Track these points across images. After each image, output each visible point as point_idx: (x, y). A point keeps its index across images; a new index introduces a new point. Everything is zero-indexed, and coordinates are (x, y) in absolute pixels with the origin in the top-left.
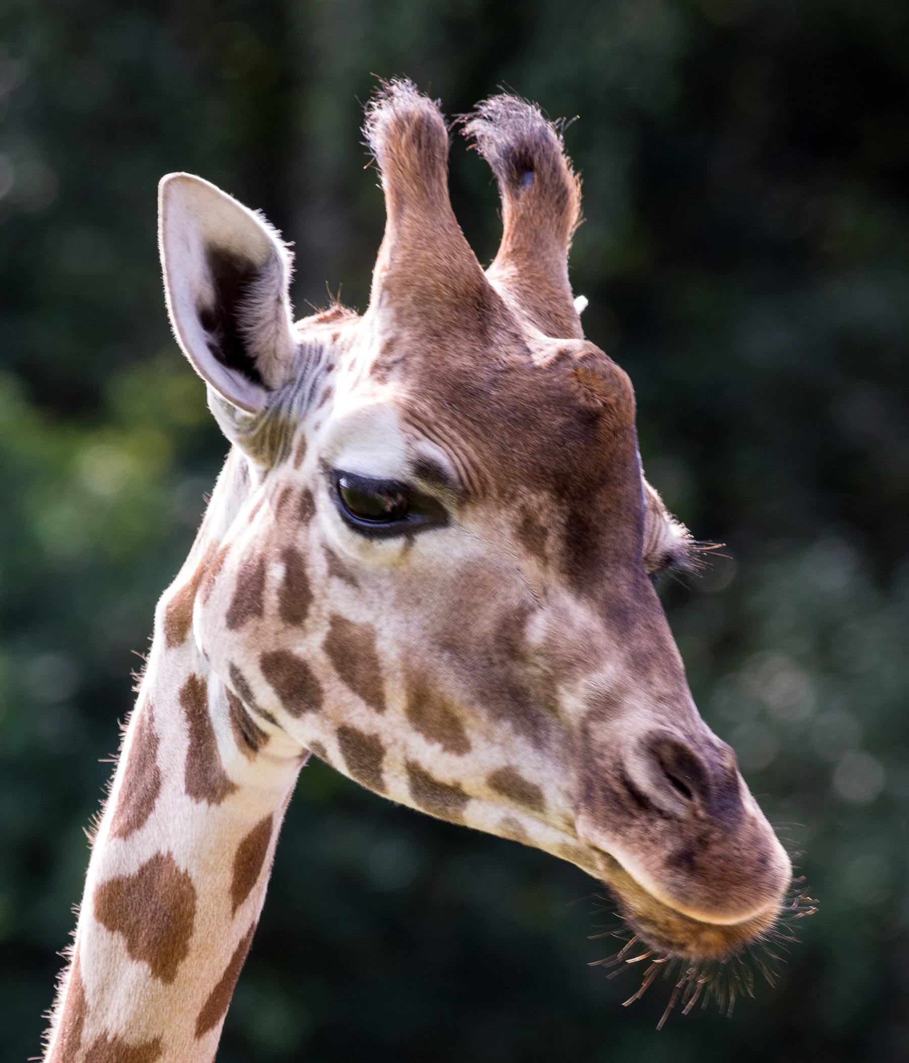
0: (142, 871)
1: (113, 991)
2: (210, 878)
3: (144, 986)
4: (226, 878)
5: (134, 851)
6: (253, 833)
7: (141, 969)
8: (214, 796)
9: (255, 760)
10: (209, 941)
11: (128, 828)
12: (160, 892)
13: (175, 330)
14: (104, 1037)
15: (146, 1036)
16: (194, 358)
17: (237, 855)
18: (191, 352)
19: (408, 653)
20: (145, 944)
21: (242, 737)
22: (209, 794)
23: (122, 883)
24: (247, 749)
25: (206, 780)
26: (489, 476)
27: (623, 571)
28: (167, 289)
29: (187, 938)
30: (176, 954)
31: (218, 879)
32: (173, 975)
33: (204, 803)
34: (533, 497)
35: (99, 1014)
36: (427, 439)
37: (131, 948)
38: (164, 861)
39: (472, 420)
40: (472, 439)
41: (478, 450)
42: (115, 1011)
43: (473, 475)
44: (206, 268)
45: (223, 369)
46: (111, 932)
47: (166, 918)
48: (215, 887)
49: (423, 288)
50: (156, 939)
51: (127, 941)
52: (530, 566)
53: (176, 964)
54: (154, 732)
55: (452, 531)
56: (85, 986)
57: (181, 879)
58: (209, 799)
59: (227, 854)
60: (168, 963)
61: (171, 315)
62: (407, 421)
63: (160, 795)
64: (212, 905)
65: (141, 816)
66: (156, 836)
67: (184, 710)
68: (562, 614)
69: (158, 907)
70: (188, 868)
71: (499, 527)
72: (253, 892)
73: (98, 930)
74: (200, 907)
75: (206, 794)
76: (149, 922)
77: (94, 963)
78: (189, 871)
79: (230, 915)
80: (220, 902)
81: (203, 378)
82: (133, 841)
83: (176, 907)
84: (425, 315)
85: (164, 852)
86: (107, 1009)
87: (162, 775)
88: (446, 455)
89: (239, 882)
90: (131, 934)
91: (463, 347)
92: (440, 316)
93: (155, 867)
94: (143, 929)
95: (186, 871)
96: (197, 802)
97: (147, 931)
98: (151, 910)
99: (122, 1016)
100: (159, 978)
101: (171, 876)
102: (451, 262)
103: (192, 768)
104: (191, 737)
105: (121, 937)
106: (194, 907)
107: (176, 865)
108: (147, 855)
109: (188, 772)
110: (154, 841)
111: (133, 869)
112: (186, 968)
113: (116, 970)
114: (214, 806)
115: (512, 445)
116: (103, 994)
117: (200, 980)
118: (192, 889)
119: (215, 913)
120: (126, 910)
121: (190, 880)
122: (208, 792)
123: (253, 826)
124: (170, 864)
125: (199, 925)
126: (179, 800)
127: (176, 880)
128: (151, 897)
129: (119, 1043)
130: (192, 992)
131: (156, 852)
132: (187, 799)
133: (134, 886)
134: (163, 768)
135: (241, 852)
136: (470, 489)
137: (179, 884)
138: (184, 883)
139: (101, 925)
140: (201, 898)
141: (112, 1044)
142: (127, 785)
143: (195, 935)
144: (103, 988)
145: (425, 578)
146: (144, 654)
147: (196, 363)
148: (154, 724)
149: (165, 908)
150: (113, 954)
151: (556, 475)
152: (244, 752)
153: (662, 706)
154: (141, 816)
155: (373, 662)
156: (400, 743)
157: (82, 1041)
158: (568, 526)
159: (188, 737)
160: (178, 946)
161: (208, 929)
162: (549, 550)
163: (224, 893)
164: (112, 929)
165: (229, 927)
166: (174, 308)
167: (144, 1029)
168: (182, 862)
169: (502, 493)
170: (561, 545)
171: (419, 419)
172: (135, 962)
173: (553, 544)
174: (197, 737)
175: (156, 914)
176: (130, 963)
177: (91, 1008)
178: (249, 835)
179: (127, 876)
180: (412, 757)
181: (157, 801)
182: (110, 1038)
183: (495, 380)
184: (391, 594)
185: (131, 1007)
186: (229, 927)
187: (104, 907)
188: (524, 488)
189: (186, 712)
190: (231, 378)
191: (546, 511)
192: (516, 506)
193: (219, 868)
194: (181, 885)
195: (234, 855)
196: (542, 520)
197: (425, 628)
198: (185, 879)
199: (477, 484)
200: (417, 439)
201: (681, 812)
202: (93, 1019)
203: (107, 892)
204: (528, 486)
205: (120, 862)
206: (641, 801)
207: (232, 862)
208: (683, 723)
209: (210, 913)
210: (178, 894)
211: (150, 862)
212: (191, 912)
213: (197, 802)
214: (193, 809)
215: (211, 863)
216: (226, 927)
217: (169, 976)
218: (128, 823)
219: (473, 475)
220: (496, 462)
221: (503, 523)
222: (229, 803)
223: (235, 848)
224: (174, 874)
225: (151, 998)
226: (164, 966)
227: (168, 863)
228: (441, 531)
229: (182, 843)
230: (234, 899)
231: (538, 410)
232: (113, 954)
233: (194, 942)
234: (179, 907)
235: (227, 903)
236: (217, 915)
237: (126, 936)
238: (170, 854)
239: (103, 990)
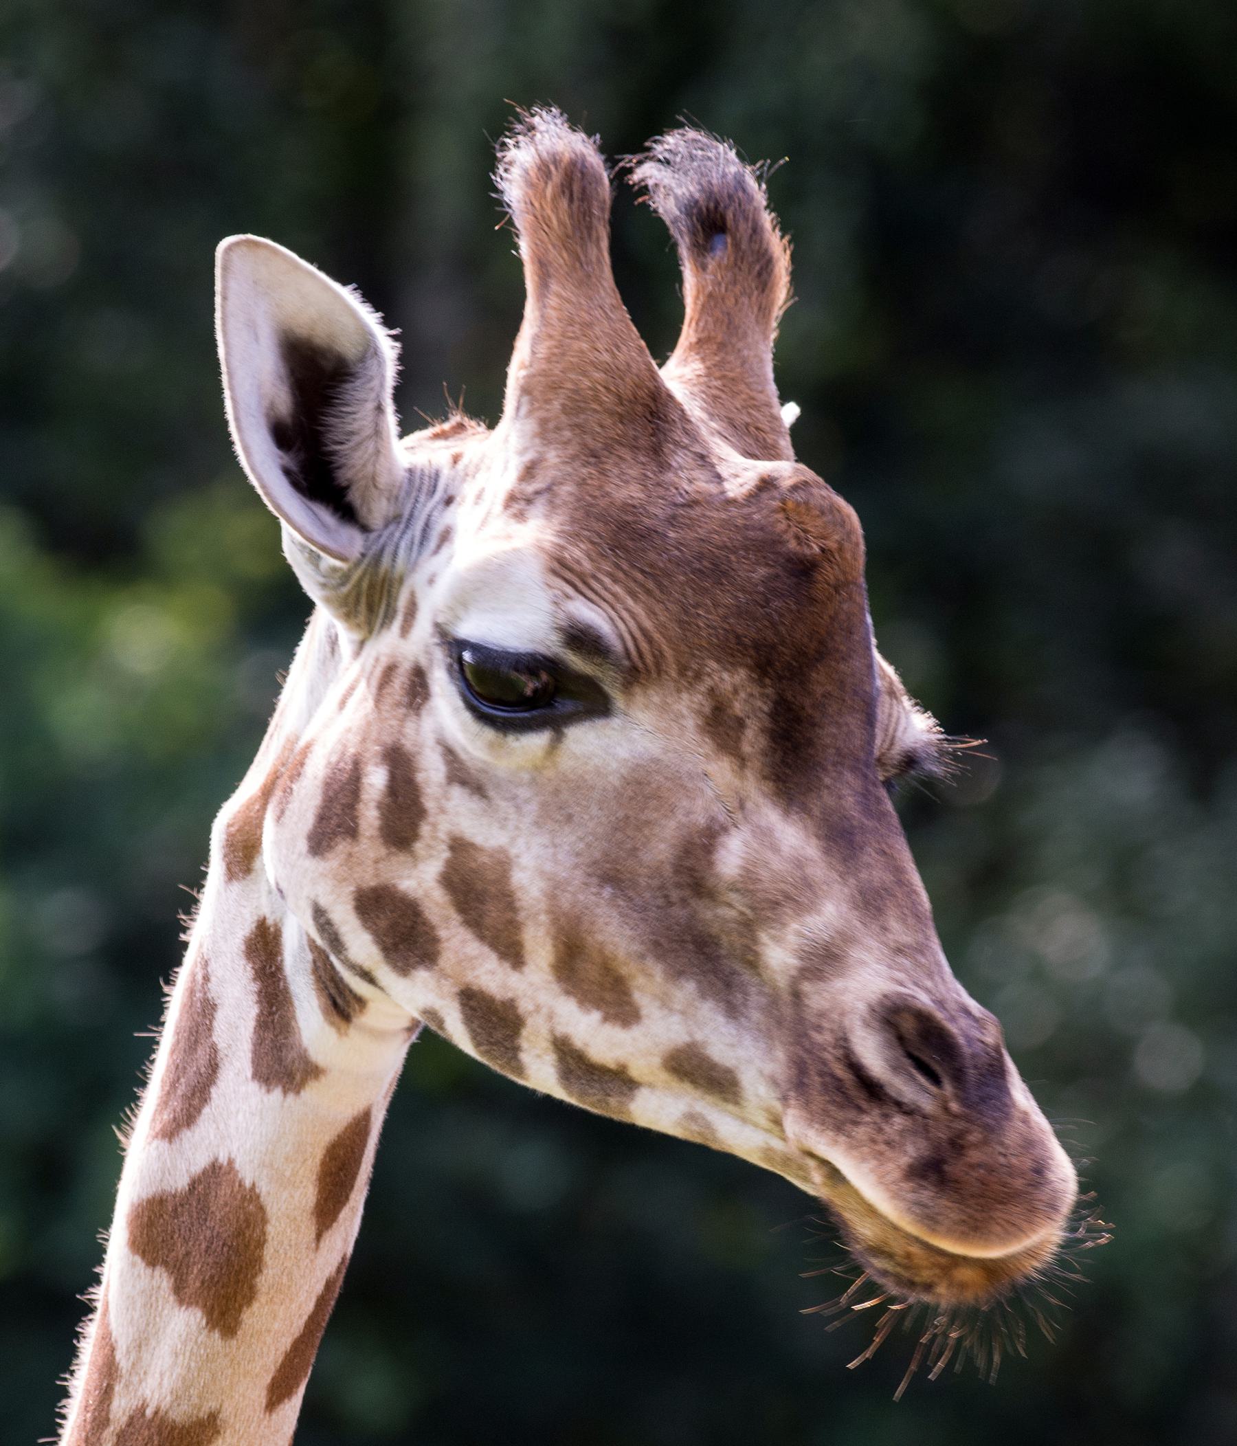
0: (193, 1185)
1: (154, 1349)
2: (285, 1195)
3: (196, 1342)
4: (307, 1194)
5: (182, 1158)
6: (344, 1133)
7: (192, 1318)
8: (292, 1083)
9: (346, 1034)
10: (285, 1280)
11: (174, 1126)
12: (217, 1213)
13: (238, 449)
14: (142, 1410)
15: (199, 1409)
16: (263, 487)
17: (323, 1163)
18: (259, 479)
19: (555, 888)
20: (198, 1284)
21: (329, 1002)
22: (285, 1080)
23: (166, 1201)
24: (337, 1019)
25: (280, 1060)
26: (665, 647)
28: (227, 394)
29: (255, 1276)
30: (239, 1297)
31: (297, 1195)
32: (236, 1326)
33: (277, 1093)
34: (726, 676)
35: (135, 1379)
36: (581, 598)
37: (179, 1289)
38: (223, 1171)
39: (643, 572)
40: (643, 597)
41: (651, 613)
42: (157, 1375)
43: (644, 646)
44: (280, 364)
45: (303, 502)
46: (152, 1268)
47: (225, 1249)
48: (293, 1207)
49: (576, 392)
50: (212, 1277)
51: (173, 1279)
52: (721, 771)
53: (240, 1311)
54: (209, 996)
55: (616, 722)
56: (116, 1341)
57: (246, 1196)
58: (284, 1087)
59: (309, 1162)
60: (229, 1309)
61: (232, 428)
62: (554, 572)
63: (218, 1082)
64: (289, 1231)
65: (192, 1109)
66: (212, 1137)
67: (251, 965)
68: (765, 835)
69: (215, 1234)
70: (256, 1181)
71: (679, 716)
72: (344, 1214)
73: (134, 1265)
74: (272, 1234)
75: (280, 1080)
76: (203, 1254)
77: (128, 1310)
78: (257, 1185)
79: (314, 1245)
80: (299, 1227)
81: (276, 514)
82: (181, 1144)
83: (239, 1233)
84: (579, 428)
85: (223, 1160)
86: (145, 1373)
87: (221, 1055)
88: (608, 619)
89: (326, 1200)
90: (178, 1270)
91: (630, 472)
92: (598, 429)
93: (212, 1180)
94: (194, 1263)
95: (254, 1184)
96: (268, 1091)
97: (199, 1266)
98: (205, 1238)
99: (165, 1382)
100: (216, 1331)
101: (232, 1191)
103: (261, 1044)
104: (259, 1002)
105: (165, 1275)
106: (264, 1233)
107: (240, 1176)
108: (200, 1162)
109: (256, 1050)
110: (210, 1144)
111: (181, 1182)
112: (253, 1317)
113: (158, 1319)
114: (291, 1097)
115: (697, 605)
116: (140, 1352)
117: (272, 1334)
118: (261, 1209)
119: (293, 1243)
120: (172, 1238)
121: (258, 1197)
122: (283, 1077)
123: (345, 1124)
124: (231, 1176)
125: (271, 1259)
126: (243, 1089)
127: (239, 1197)
128: (206, 1220)
129: (162, 1419)
130: (261, 1349)
131: (212, 1159)
132: (254, 1087)
133: (182, 1205)
134: (221, 1045)
135: (328, 1159)
136: (640, 665)
137: (243, 1203)
138: (251, 1201)
139: (138, 1259)
140: (273, 1221)
141: (152, 1420)
142: (173, 1068)
143: (265, 1272)
144: (141, 1344)
145: (579, 786)
147: (267, 494)
148: (209, 985)
149: (225, 1235)
150: (154, 1298)
151: (757, 646)
152: (332, 1024)
153: (902, 960)
154: (192, 1109)
156: (544, 1010)
157: (111, 1417)
158: (773, 715)
159: (256, 1003)
160: (242, 1286)
161: (283, 1264)
162: (746, 748)
163: (305, 1214)
164: (152, 1263)
165: (312, 1261)
166: (237, 419)
167: (195, 1400)
168: (248, 1173)
169: (682, 670)
170: (763, 742)
171: (571, 570)
172: (183, 1308)
173: (753, 740)
174: (268, 1003)
175: (212, 1243)
176: (176, 1309)
177: (124, 1371)
178: (338, 1136)
179: (173, 1192)
180: (561, 1030)
181: (213, 1090)
182: (149, 1412)
183: (674, 517)
184: (532, 809)
185: (178, 1370)
186: (312, 1261)
187: (142, 1233)
188: (713, 664)
189: (253, 968)
190: (314, 514)
191: (743, 695)
192: (702, 688)
193: (298, 1181)
194: (246, 1204)
195: (318, 1163)
196: (738, 708)
197: (578, 855)
198: (252, 1196)
199: (649, 659)
200: (568, 597)
201: (927, 1104)
202: (127, 1386)
203: (146, 1213)
204: (718, 661)
205: (163, 1173)
207: (315, 1172)
209: (286, 1242)
210: (242, 1216)
211: (205, 1172)
212: (259, 1241)
213: (268, 1091)
214: (262, 1101)
215: (288, 1174)
216: (308, 1260)
217: (230, 1327)
218: (175, 1119)
219: (644, 646)
220: (675, 629)
221: (685, 712)
222: (312, 1092)
223: (319, 1154)
224: (236, 1188)
225: (205, 1357)
226: (223, 1314)
227: (229, 1173)
228: (600, 723)
229: (248, 1146)
230: (318, 1223)
231: (733, 558)
232: (154, 1298)
233: (264, 1281)
234: (244, 1234)
235: (308, 1228)
236: (296, 1244)
237: (172, 1273)
238: (231, 1162)
239: (140, 1346)
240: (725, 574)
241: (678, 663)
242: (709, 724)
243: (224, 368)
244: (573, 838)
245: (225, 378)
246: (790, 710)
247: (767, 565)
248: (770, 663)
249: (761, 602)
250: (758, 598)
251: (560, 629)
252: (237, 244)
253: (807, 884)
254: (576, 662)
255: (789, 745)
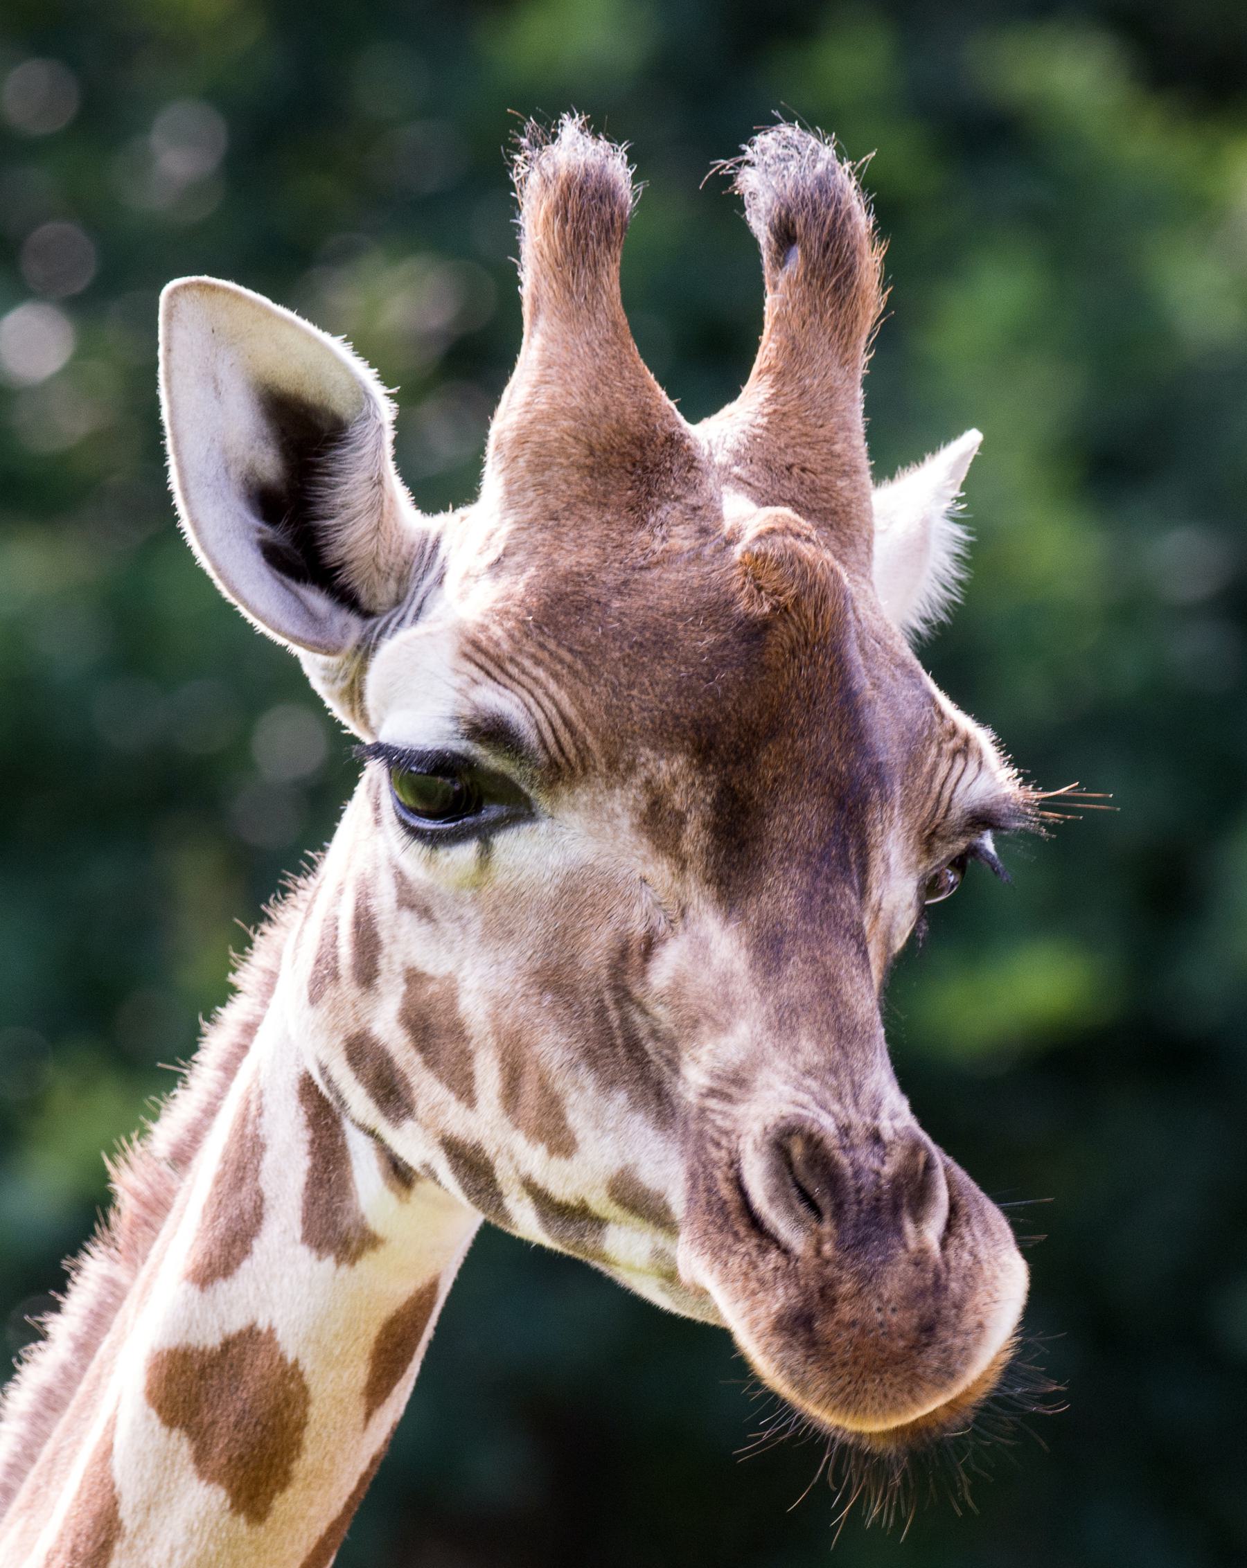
0: (227, 1344)
1: (165, 1517)
2: (332, 1375)
3: (217, 1524)
4: (359, 1373)
5: (214, 1311)
8: (346, 1252)
9: (408, 1202)
10: (326, 1466)
11: (208, 1272)
12: (251, 1384)
13: (185, 524)
16: (217, 569)
17: (378, 1341)
18: (211, 558)
19: (500, 1003)
20: (224, 1460)
21: (390, 1165)
22: (339, 1248)
23: (191, 1356)
24: (398, 1186)
25: (334, 1225)
27: (795, 874)
29: (291, 1461)
30: (272, 1482)
31: (346, 1375)
32: (265, 1512)
35: (139, 1543)
36: (490, 682)
37: (200, 1457)
38: (262, 1338)
39: (570, 650)
40: (567, 678)
41: (575, 697)
42: (167, 1547)
43: (565, 737)
44: (262, 423)
45: (282, 582)
46: (168, 1429)
47: (259, 1428)
48: (341, 1387)
49: (542, 445)
50: (241, 1457)
51: (194, 1447)
52: (660, 871)
53: (271, 1498)
54: (261, 1132)
55: (543, 827)
56: (120, 1494)
57: (287, 1372)
58: (337, 1256)
60: (258, 1495)
61: (178, 500)
63: (262, 1235)
64: (334, 1413)
65: (230, 1259)
67: (304, 1109)
68: (701, 948)
69: (247, 1407)
70: (299, 1357)
71: (613, 816)
72: (397, 1390)
73: (148, 1418)
74: (314, 1417)
75: (333, 1248)
76: (232, 1428)
77: (137, 1464)
78: (300, 1362)
79: (361, 1426)
80: (346, 1408)
81: (232, 600)
82: (214, 1296)
83: (276, 1412)
85: (262, 1325)
86: (152, 1540)
87: (267, 1204)
89: (379, 1378)
90: (202, 1438)
93: (248, 1346)
94: (221, 1436)
96: (319, 1259)
97: (226, 1441)
98: (235, 1410)
100: (242, 1515)
101: (271, 1364)
102: (623, 624)
103: (314, 1204)
104: (313, 1153)
106: (305, 1415)
107: (281, 1349)
108: (236, 1324)
109: (308, 1209)
110: (248, 1303)
111: (213, 1341)
112: (285, 1504)
113: (172, 1486)
114: (344, 1268)
115: (631, 686)
116: (148, 1516)
117: (306, 1521)
118: (304, 1389)
119: (338, 1425)
120: (197, 1400)
121: (301, 1375)
122: (337, 1245)
123: (404, 1299)
124: (271, 1346)
125: (312, 1442)
127: (279, 1371)
128: (237, 1388)
130: (293, 1537)
131: (250, 1323)
132: (304, 1253)
133: (212, 1366)
134: (268, 1194)
135: (384, 1337)
137: (284, 1379)
139: (153, 1413)
142: (216, 1201)
143: (303, 1457)
145: (515, 898)
146: (252, 928)
147: (221, 577)
148: (262, 1120)
149: (260, 1412)
150: (169, 1462)
151: (696, 726)
152: (392, 1189)
154: (230, 1259)
155: (457, 1031)
158: (717, 806)
159: (309, 1154)
160: (276, 1471)
161: (325, 1448)
162: (687, 847)
163: (354, 1395)
164: (170, 1421)
165: (358, 1442)
166: (185, 490)
168: (290, 1346)
169: (612, 765)
170: (705, 839)
171: (485, 653)
172: (204, 1483)
173: (694, 836)
174: (324, 1157)
175: (243, 1418)
176: (195, 1481)
177: (128, 1531)
178: (398, 1312)
179: (201, 1348)
180: (524, 1170)
184: (476, 926)
185: (192, 1551)
186: (358, 1442)
187: (159, 1388)
188: (647, 752)
189: (306, 1112)
191: (682, 785)
192: (638, 780)
193: (348, 1361)
194: (286, 1382)
195: (373, 1341)
196: (678, 800)
199: (572, 753)
200: (475, 682)
201: (798, 1241)
202: (130, 1548)
203: (166, 1364)
204: (654, 748)
205: (190, 1326)
206: (755, 1223)
207: (368, 1351)
208: (836, 1107)
209: (330, 1425)
210: (281, 1394)
211: (241, 1334)
212: (299, 1422)
213: (319, 1259)
214: (312, 1269)
215: (337, 1352)
216: (354, 1442)
217: (258, 1513)
218: (210, 1264)
219: (565, 737)
221: (619, 810)
222: (368, 1264)
223: (374, 1331)
225: (226, 1542)
226: (251, 1498)
227: (269, 1343)
228: (526, 828)
229: (293, 1317)
230: (368, 1402)
232: (169, 1462)
233: (302, 1466)
234: (282, 1414)
235: (357, 1408)
236: (341, 1427)
237: (194, 1439)
238: (271, 1331)
239: (149, 1509)
240: (668, 645)
241: (606, 753)
242: (645, 822)
243: (168, 431)
244: (515, 954)
245: (169, 442)
246: (735, 799)
247: (717, 630)
248: (711, 745)
249: (705, 675)
250: (704, 671)
251: (456, 719)
252: (186, 287)
253: (727, 1002)
254: (490, 759)
255: (735, 842)
